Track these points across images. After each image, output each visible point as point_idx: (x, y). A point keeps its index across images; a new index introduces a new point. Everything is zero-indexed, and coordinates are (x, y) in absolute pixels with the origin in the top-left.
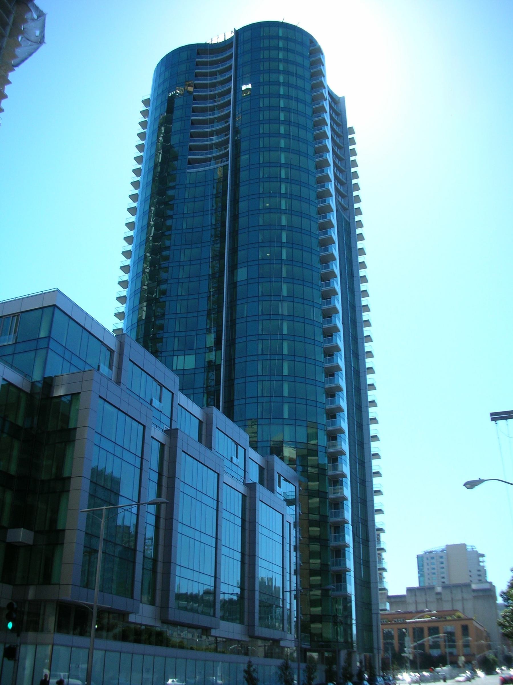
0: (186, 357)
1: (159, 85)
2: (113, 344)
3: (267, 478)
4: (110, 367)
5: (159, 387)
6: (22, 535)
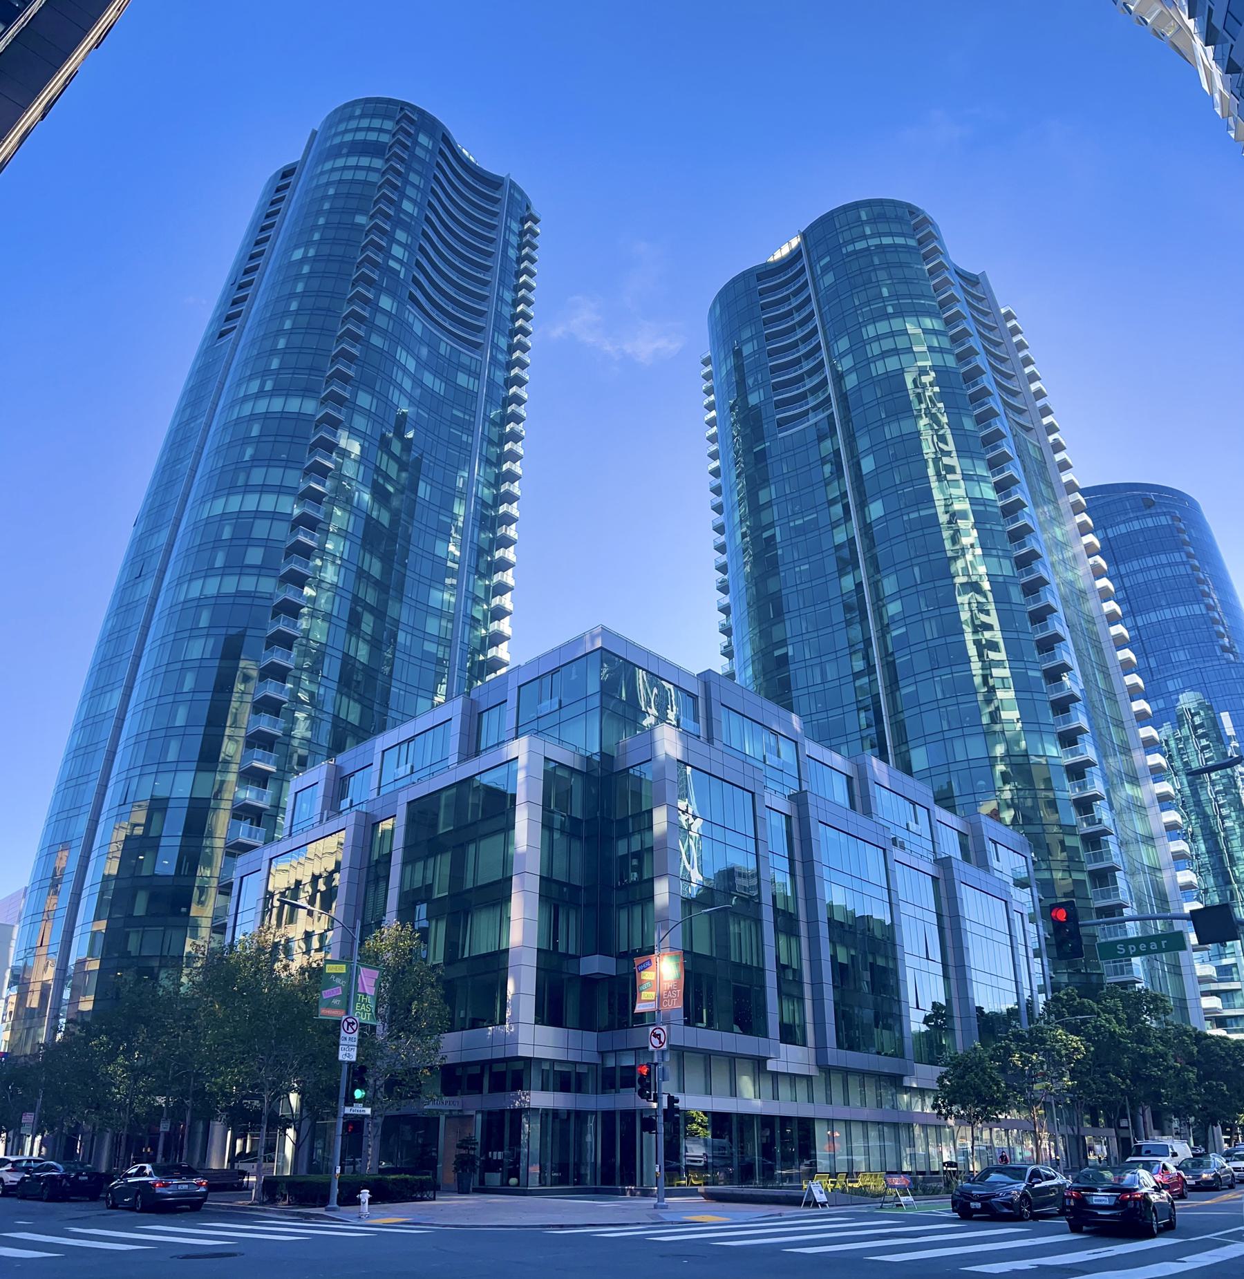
0: (271, 470)
1: (191, 391)
2: (696, 689)
3: (974, 849)
5: (772, 738)
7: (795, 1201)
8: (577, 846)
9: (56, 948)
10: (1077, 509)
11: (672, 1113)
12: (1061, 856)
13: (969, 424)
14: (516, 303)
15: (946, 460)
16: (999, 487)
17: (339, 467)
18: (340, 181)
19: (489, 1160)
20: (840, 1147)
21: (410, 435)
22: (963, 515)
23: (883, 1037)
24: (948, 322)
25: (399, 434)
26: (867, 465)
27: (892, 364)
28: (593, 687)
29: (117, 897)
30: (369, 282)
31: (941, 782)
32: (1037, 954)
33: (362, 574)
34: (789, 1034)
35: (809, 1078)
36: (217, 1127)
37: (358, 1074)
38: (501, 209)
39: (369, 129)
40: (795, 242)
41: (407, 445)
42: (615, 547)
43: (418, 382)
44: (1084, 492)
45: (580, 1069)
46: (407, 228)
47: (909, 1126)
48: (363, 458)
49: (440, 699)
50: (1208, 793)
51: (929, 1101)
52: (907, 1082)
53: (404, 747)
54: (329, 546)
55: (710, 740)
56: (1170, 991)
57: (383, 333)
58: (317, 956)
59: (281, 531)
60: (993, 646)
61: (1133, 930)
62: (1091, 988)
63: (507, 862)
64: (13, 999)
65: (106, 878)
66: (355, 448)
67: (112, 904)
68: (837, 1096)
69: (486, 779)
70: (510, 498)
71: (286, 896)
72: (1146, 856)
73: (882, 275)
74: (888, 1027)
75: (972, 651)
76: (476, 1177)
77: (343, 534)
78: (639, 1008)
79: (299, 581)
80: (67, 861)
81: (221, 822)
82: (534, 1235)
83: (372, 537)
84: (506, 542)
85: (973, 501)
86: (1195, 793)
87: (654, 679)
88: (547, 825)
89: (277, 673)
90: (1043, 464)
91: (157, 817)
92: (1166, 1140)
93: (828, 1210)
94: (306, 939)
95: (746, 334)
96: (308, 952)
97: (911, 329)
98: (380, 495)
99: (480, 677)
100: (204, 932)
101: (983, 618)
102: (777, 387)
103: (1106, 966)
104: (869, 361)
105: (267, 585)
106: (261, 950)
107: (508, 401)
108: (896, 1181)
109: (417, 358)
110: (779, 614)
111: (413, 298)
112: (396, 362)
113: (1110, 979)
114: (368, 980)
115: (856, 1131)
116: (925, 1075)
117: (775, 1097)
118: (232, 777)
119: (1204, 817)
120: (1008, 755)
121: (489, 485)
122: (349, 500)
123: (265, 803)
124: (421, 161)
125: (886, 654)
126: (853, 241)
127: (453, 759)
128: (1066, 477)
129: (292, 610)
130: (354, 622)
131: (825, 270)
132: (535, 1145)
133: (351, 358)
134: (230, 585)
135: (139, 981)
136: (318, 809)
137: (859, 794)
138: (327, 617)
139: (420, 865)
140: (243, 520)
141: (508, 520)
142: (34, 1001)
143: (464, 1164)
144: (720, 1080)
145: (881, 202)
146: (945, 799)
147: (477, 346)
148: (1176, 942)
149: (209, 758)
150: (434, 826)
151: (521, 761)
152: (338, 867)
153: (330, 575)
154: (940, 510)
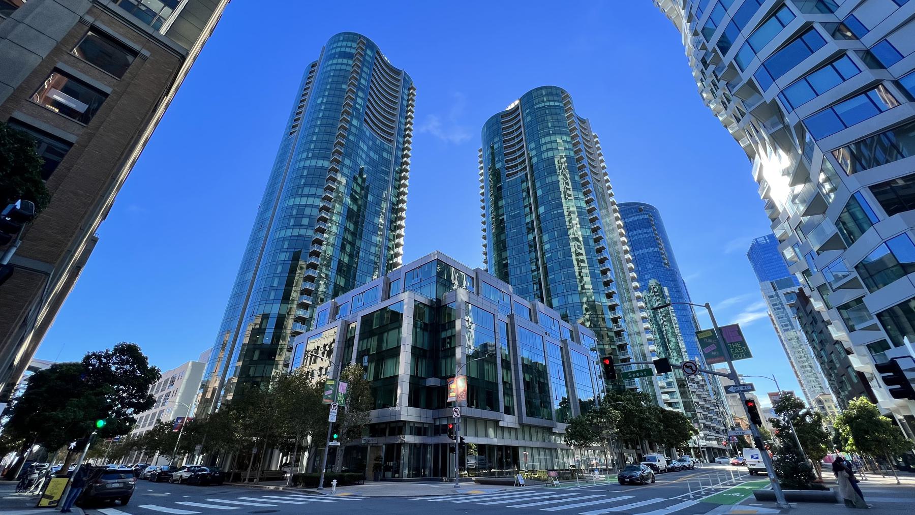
2: (474, 276)
7: (511, 484)
8: (426, 334)
9: (221, 373)
10: (615, 211)
11: (462, 444)
12: (607, 339)
13: (577, 178)
14: (406, 124)
15: (568, 192)
16: (587, 202)
17: (338, 188)
18: (335, 70)
19: (387, 466)
20: (529, 459)
21: (365, 176)
22: (574, 212)
23: (544, 411)
24: (572, 138)
25: (361, 175)
26: (539, 193)
27: (550, 154)
28: (434, 274)
29: (248, 353)
30: (348, 113)
31: (563, 311)
32: (600, 377)
33: (346, 229)
34: (508, 411)
35: (516, 429)
36: (276, 452)
37: (336, 427)
38: (401, 84)
39: (346, 47)
40: (517, 102)
41: (364, 180)
42: (443, 223)
43: (368, 155)
44: (618, 205)
45: (427, 426)
46: (363, 91)
47: (556, 449)
48: (347, 185)
49: (375, 277)
50: (660, 316)
51: (563, 439)
52: (554, 430)
54: (334, 218)
55: (478, 294)
56: (650, 391)
57: (355, 135)
58: (324, 377)
59: (315, 212)
60: (583, 261)
61: (634, 368)
62: (621, 390)
63: (399, 340)
64: (201, 395)
65: (244, 345)
66: (344, 181)
67: (245, 355)
68: (527, 437)
69: (391, 308)
70: (403, 202)
71: (314, 355)
72: (638, 340)
73: (549, 118)
74: (545, 407)
75: (575, 263)
76: (381, 474)
77: (339, 213)
78: (449, 400)
79: (322, 231)
80: (229, 338)
81: (290, 323)
82: (402, 501)
83: (350, 215)
84: (401, 218)
85: (578, 207)
86: (655, 317)
87: (457, 270)
88: (415, 326)
89: (314, 266)
90: (603, 194)
91: (265, 321)
92: (655, 454)
93: (525, 487)
94: (320, 370)
95: (496, 140)
96: (320, 376)
97: (558, 140)
98: (354, 199)
99: (391, 269)
100: (280, 367)
101: (579, 251)
102: (507, 161)
103: (626, 382)
104: (542, 152)
105: (310, 233)
106: (301, 375)
107: (403, 164)
108: (552, 474)
109: (368, 145)
110: (505, 247)
111: (365, 120)
112: (359, 147)
113: (628, 387)
114: (343, 387)
115: (535, 452)
116: (561, 427)
117: (503, 437)
118: (295, 306)
119: (658, 325)
120: (588, 301)
121: (395, 196)
122: (341, 201)
123: (307, 316)
124: (368, 62)
125: (544, 263)
126: (539, 103)
128: (611, 199)
129: (319, 242)
130: (343, 248)
131: (527, 115)
132: (406, 459)
133: (342, 145)
134: (296, 232)
135: (252, 387)
137: (533, 315)
138: (333, 245)
139: (365, 341)
140: (301, 208)
141: (402, 210)
142: (209, 396)
143: (377, 468)
144: (481, 430)
145: (551, 87)
146: (565, 318)
147: (391, 141)
148: (649, 373)
149: (286, 298)
150: (372, 326)
151: (406, 302)
152: (334, 342)
153: (334, 229)
154: (565, 210)
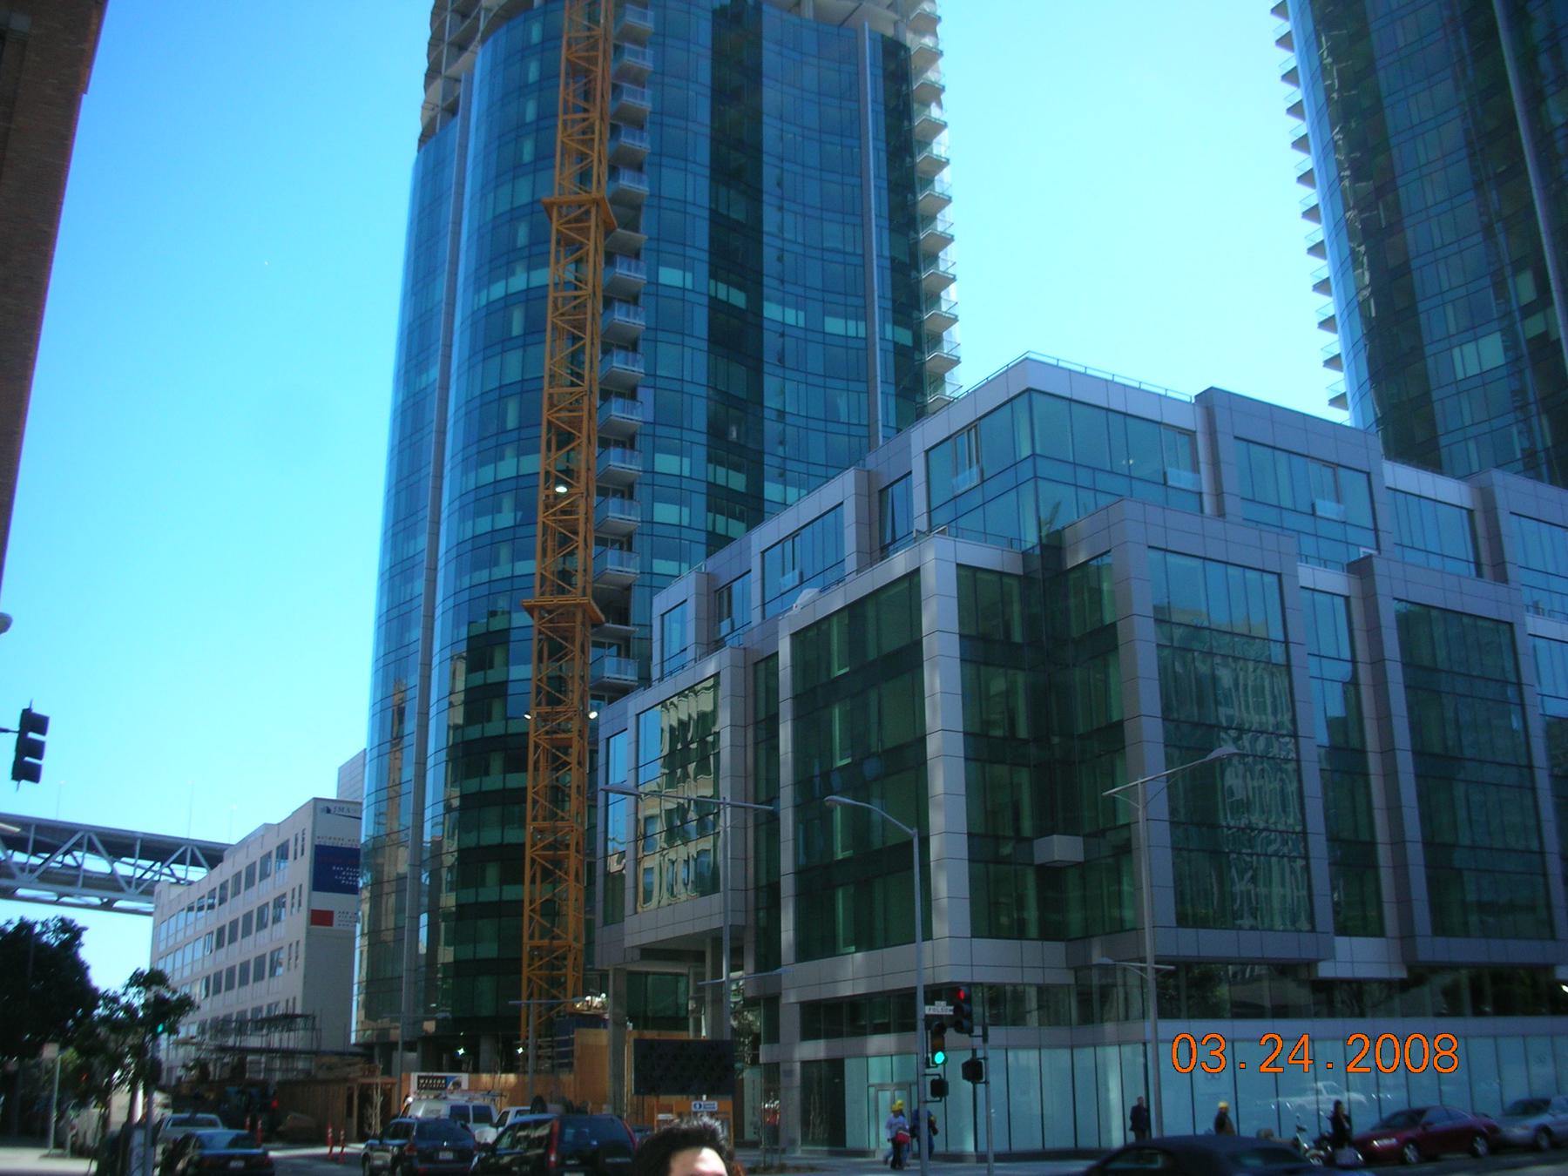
4: (1195, 468)
5: (1327, 473)
6: (1062, 848)
53: (789, 544)
127: (851, 563)
136: (691, 637)
